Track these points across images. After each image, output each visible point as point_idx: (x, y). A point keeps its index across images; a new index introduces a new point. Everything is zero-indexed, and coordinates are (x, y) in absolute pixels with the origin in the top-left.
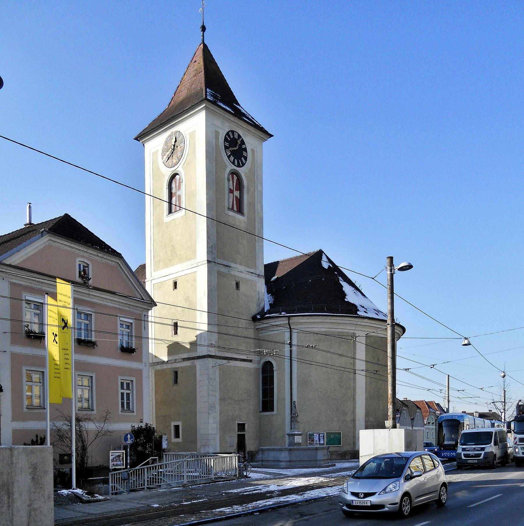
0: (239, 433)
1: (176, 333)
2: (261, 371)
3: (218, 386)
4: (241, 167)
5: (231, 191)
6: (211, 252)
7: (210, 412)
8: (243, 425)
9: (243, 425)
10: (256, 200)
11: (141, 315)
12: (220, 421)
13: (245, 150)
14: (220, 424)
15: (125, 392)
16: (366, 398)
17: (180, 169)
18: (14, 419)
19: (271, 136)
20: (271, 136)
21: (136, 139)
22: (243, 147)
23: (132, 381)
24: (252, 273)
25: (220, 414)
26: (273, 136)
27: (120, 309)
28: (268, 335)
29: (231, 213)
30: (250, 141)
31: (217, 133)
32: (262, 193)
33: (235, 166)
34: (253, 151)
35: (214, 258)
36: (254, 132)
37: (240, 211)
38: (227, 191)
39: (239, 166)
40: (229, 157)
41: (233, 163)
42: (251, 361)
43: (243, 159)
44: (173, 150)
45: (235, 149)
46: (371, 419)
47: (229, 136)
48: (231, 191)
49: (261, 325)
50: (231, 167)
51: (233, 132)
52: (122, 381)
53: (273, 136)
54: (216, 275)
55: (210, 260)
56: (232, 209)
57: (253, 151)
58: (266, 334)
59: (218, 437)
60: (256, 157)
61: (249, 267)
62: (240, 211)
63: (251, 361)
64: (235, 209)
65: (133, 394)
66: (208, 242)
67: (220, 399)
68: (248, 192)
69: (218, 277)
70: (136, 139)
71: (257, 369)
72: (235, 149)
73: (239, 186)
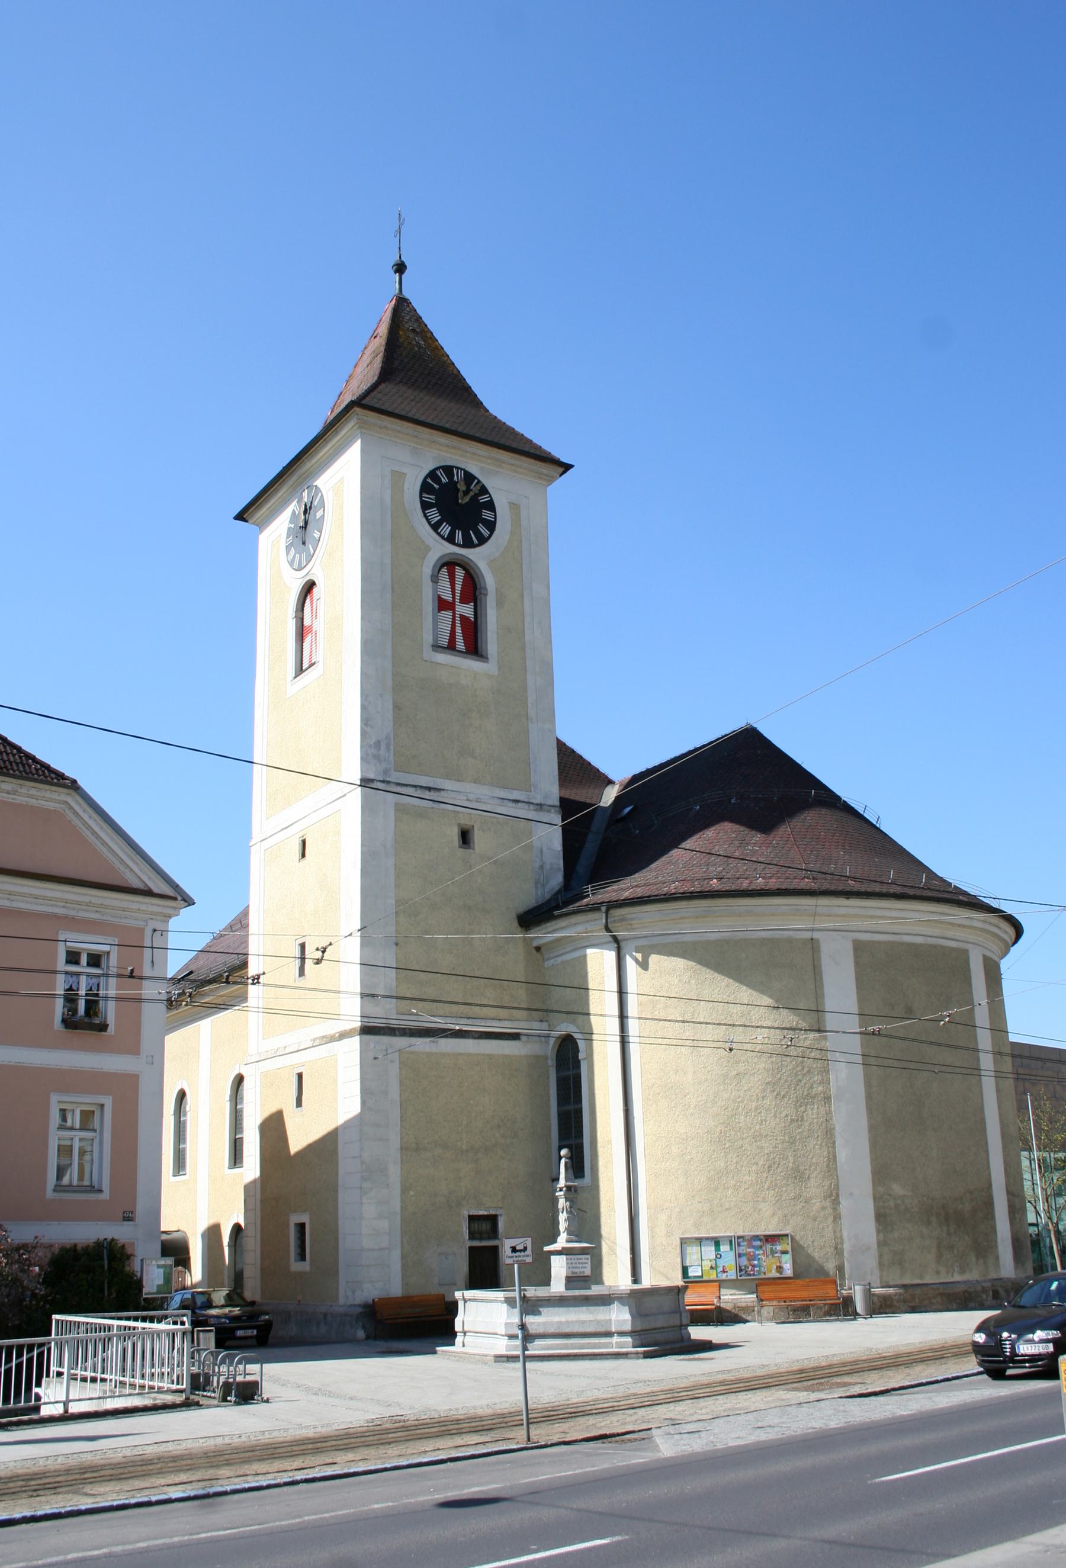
0: (476, 1243)
1: (302, 972)
2: (551, 1062)
3: (395, 1114)
4: (473, 546)
5: (443, 605)
6: (377, 757)
7: (367, 1185)
8: (493, 1219)
9: (493, 1219)
10: (527, 620)
11: (141, 931)
12: (403, 1208)
13: (491, 506)
14: (403, 1220)
15: (77, 1139)
16: (872, 1128)
17: (316, 571)
18: (470, 1238)
19: (567, 467)
20: (567, 467)
21: (241, 517)
22: (483, 499)
23: (102, 1106)
24: (517, 801)
25: (404, 1190)
26: (572, 466)
27: (66, 917)
28: (562, 962)
29: (443, 658)
30: (502, 482)
31: (398, 478)
32: (547, 602)
33: (458, 545)
34: (514, 507)
35: (386, 772)
36: (512, 461)
37: (474, 648)
38: (428, 605)
39: (468, 544)
40: (435, 527)
41: (451, 539)
42: (515, 1037)
43: (481, 528)
44: (304, 530)
45: (457, 507)
46: (897, 1189)
47: (437, 480)
48: (443, 605)
49: (544, 935)
50: (440, 549)
51: (448, 470)
52: (64, 1106)
53: (572, 466)
54: (392, 813)
55: (372, 776)
56: (451, 646)
57: (514, 507)
58: (559, 960)
59: (396, 1254)
60: (524, 523)
61: (505, 787)
62: (474, 648)
63: (515, 1037)
64: (460, 644)
65: (101, 1143)
66: (364, 734)
67: (404, 1149)
68: (500, 603)
69: (397, 820)
70: (241, 517)
71: (537, 1057)
72: (457, 507)
73: (472, 590)
